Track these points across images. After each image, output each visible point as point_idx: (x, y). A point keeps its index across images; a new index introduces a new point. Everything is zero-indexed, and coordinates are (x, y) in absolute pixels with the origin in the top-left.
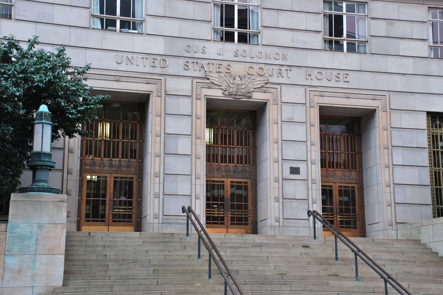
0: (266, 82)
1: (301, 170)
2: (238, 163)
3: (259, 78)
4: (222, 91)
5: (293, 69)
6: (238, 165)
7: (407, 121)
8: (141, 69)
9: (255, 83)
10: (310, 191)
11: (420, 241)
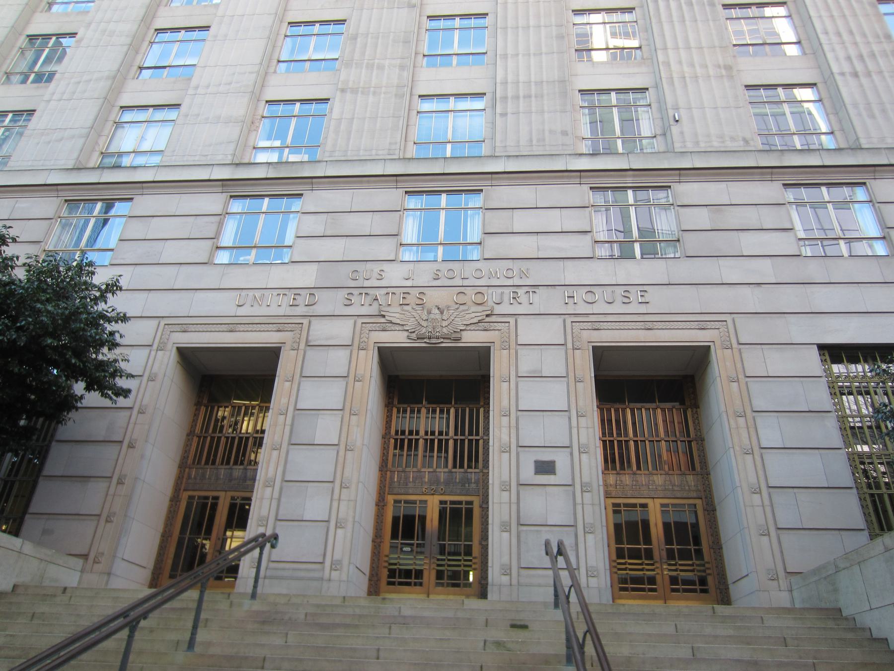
0: (489, 312)
1: (559, 466)
2: (455, 466)
4: (406, 334)
5: (539, 291)
6: (454, 470)
7: (778, 363)
8: (274, 310)
10: (579, 508)
11: (840, 610)
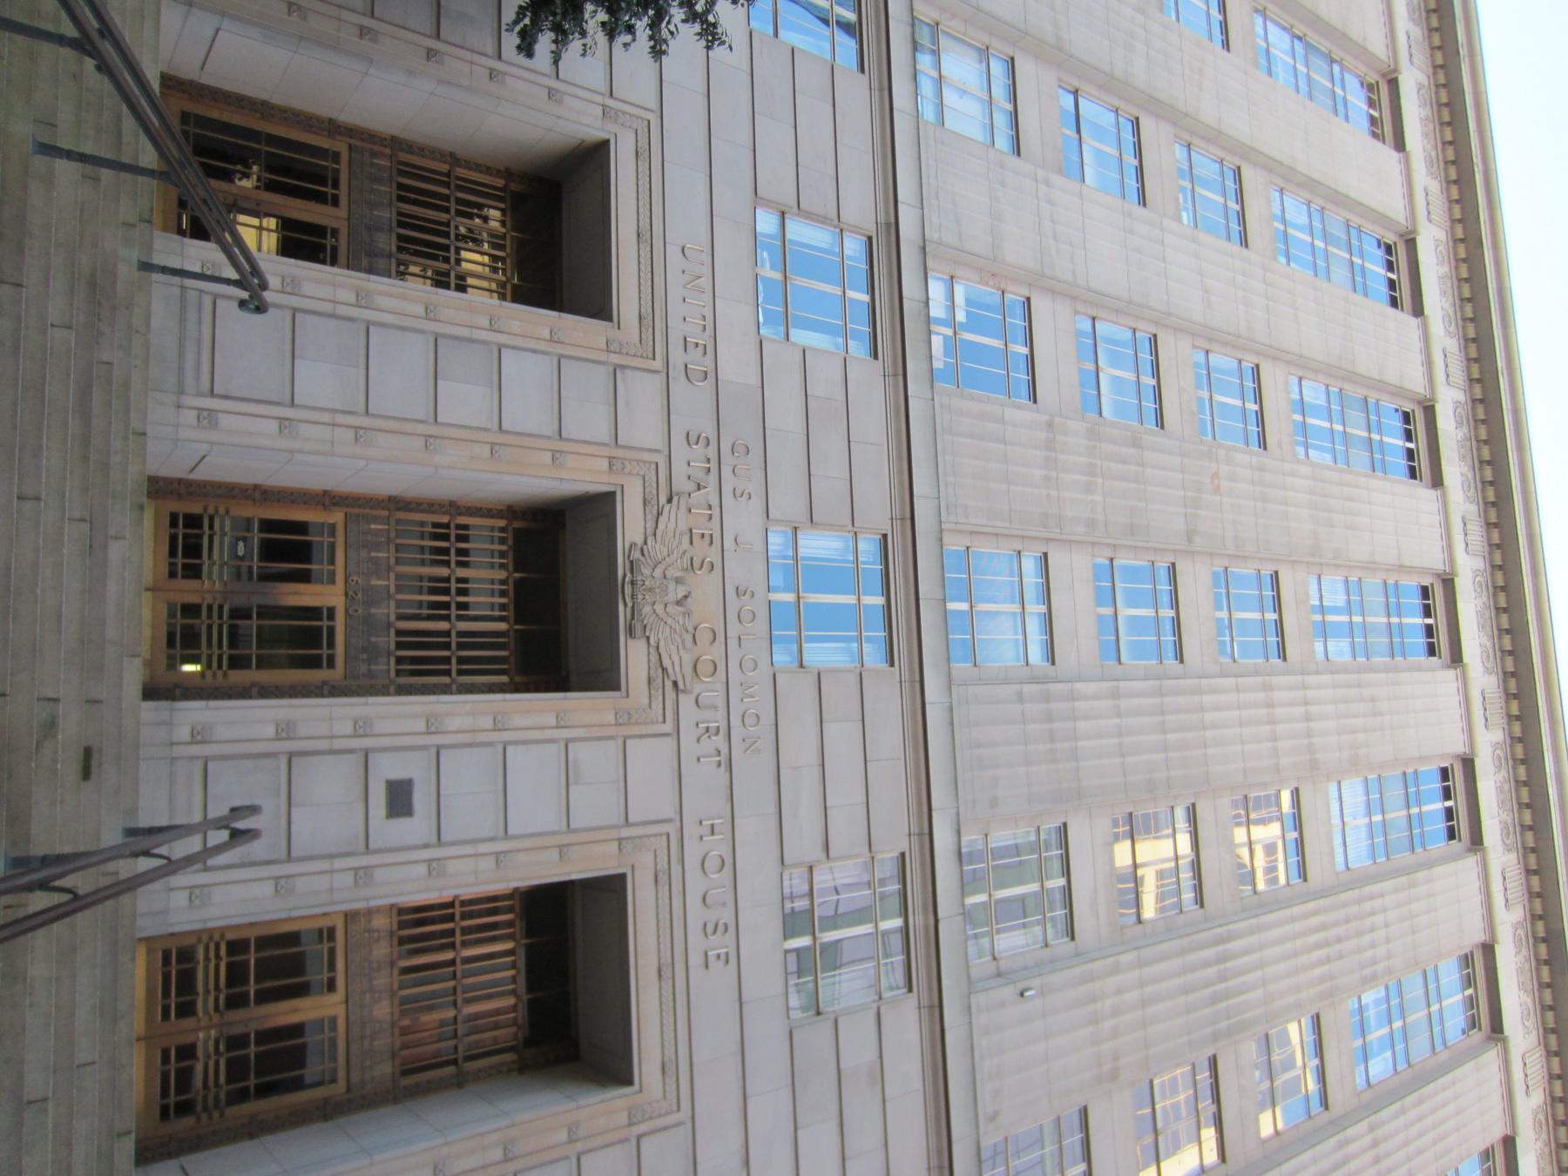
0: (681, 686)
1: (403, 823)
2: (399, 633)
3: (688, 660)
4: (640, 541)
9: (673, 648)
